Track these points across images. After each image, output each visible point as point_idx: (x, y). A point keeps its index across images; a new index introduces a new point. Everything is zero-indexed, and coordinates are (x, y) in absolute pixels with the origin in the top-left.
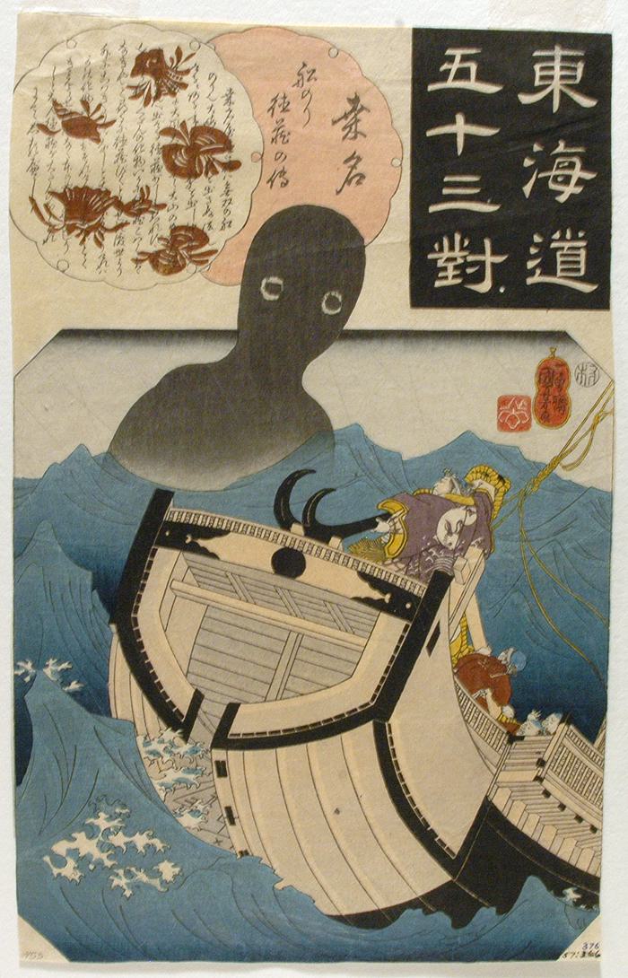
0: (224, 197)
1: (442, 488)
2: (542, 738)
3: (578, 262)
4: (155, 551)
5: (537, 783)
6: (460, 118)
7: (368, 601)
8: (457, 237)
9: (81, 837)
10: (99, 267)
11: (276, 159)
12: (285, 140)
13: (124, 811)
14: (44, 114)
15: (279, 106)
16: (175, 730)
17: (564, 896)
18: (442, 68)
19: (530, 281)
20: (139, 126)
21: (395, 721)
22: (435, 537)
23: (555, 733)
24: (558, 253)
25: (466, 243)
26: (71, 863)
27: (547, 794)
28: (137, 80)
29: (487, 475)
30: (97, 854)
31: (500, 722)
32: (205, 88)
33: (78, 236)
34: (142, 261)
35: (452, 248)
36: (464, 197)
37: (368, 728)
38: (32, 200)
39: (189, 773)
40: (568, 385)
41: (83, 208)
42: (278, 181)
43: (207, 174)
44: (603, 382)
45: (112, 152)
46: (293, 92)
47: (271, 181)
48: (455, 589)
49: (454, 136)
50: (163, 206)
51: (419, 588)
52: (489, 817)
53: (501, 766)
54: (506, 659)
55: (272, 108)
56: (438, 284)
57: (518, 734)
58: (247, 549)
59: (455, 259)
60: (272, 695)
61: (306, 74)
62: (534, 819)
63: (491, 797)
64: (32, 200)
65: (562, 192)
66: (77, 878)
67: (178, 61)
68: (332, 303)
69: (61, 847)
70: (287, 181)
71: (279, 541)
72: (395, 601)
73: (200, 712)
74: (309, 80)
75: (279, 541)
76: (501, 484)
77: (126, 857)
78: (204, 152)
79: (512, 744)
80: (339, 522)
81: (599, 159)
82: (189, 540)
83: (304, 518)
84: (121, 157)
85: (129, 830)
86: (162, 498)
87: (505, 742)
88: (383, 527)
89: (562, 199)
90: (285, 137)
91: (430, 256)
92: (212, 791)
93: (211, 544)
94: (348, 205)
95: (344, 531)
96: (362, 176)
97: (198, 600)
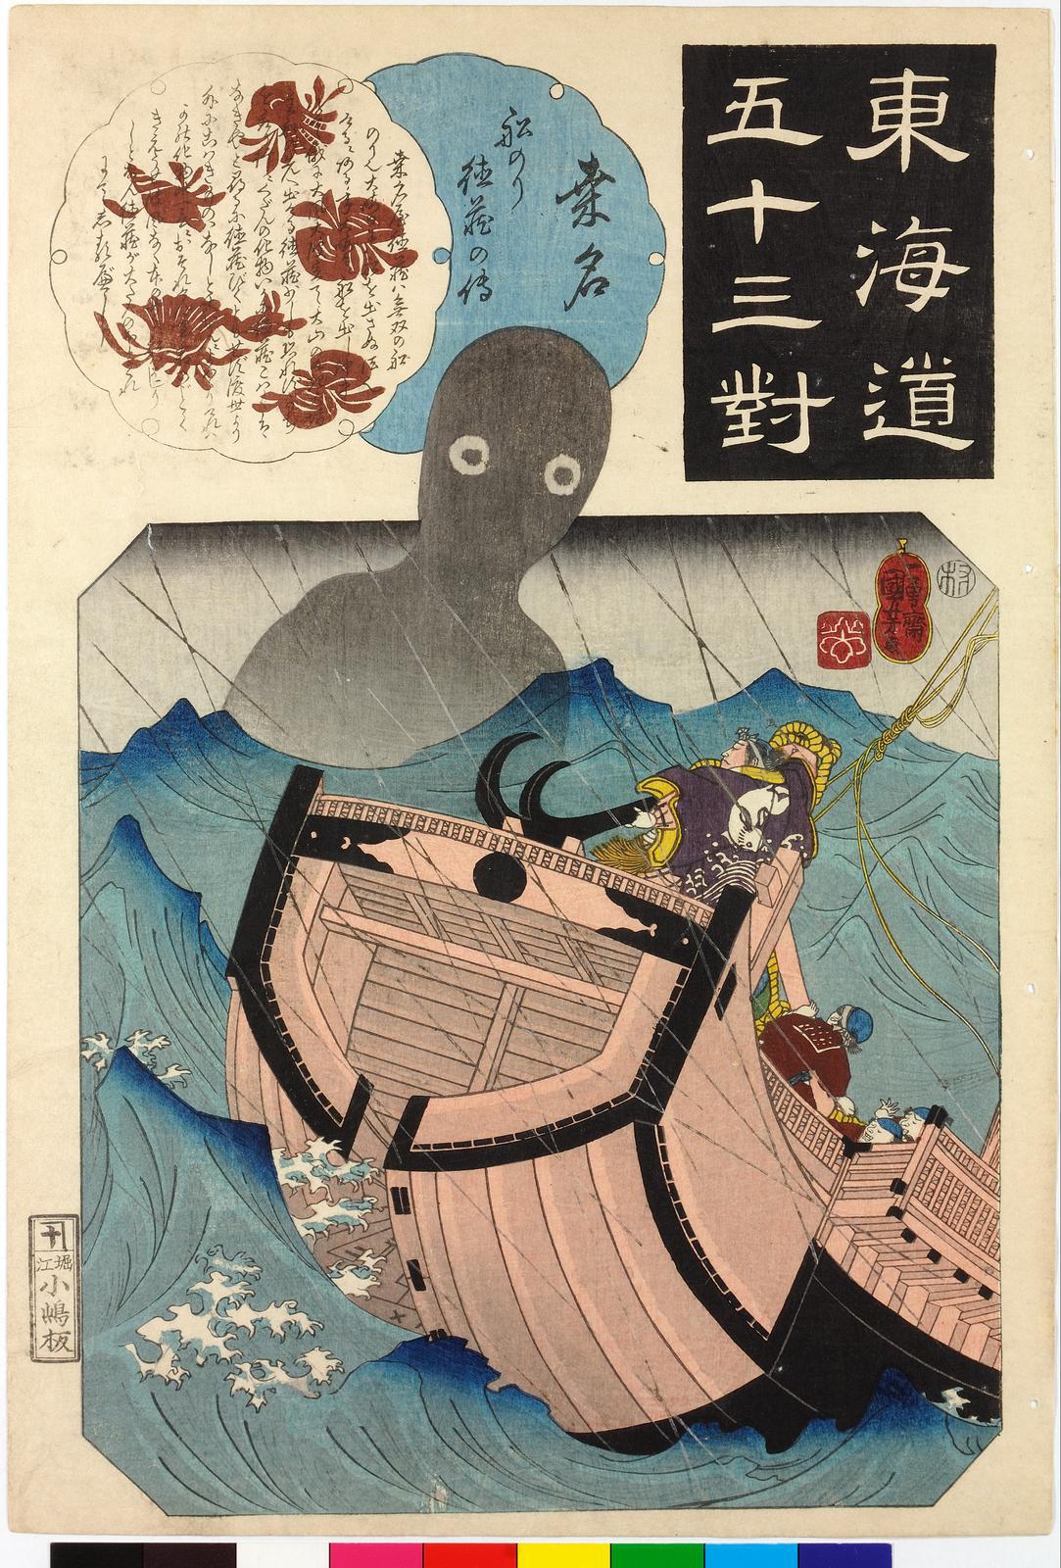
0: (395, 319)
1: (735, 760)
2: (902, 1147)
3: (944, 405)
4: (296, 861)
5: (893, 1219)
6: (757, 185)
7: (622, 935)
8: (756, 370)
9: (184, 1312)
10: (205, 429)
11: (472, 260)
12: (486, 229)
13: (250, 1270)
14: (121, 189)
15: (476, 177)
16: (327, 1141)
17: (943, 1400)
18: (729, 109)
19: (869, 435)
20: (262, 205)
21: (668, 1119)
22: (725, 834)
23: (919, 1139)
24: (912, 391)
25: (770, 377)
26: (169, 1355)
27: (909, 1236)
28: (253, 133)
29: (803, 737)
30: (210, 1340)
31: (833, 1122)
32: (360, 155)
33: (170, 372)
34: (271, 407)
35: (748, 389)
36: (764, 308)
37: (628, 1132)
38: (101, 319)
39: (352, 1208)
40: (927, 595)
41: (180, 332)
42: (475, 293)
43: (365, 274)
44: (980, 591)
45: (222, 254)
46: (497, 157)
47: (464, 292)
48: (759, 916)
49: (749, 212)
50: (299, 323)
51: (700, 913)
52: (820, 1281)
53: (836, 1192)
54: (839, 1023)
55: (465, 180)
56: (728, 442)
57: (862, 1140)
58: (443, 857)
59: (752, 404)
60: (479, 1082)
61: (516, 129)
62: (891, 1275)
63: (823, 1241)
64: (101, 319)
65: (919, 296)
66: (177, 1377)
67: (318, 100)
68: (563, 476)
69: (154, 1329)
70: (490, 291)
71: (486, 845)
72: (663, 934)
73: (368, 1112)
74: (519, 136)
75: (486, 845)
76: (826, 750)
77: (251, 1343)
78: (359, 242)
79: (851, 1157)
80: (578, 812)
81: (973, 241)
82: (347, 843)
83: (520, 811)
84: (236, 260)
85: (254, 1297)
86: (306, 779)
87: (841, 1153)
88: (644, 820)
89: (917, 306)
90: (484, 223)
91: (715, 400)
92: (388, 1235)
93: (381, 851)
94: (586, 324)
95: (584, 827)
96: (605, 282)
97: (358, 935)
